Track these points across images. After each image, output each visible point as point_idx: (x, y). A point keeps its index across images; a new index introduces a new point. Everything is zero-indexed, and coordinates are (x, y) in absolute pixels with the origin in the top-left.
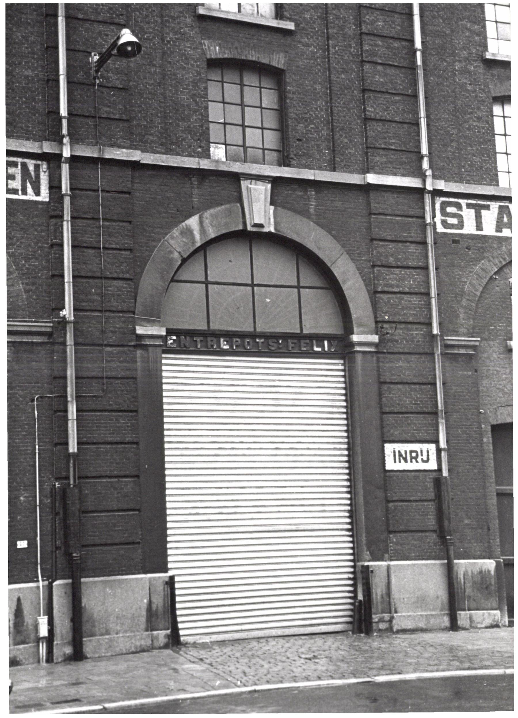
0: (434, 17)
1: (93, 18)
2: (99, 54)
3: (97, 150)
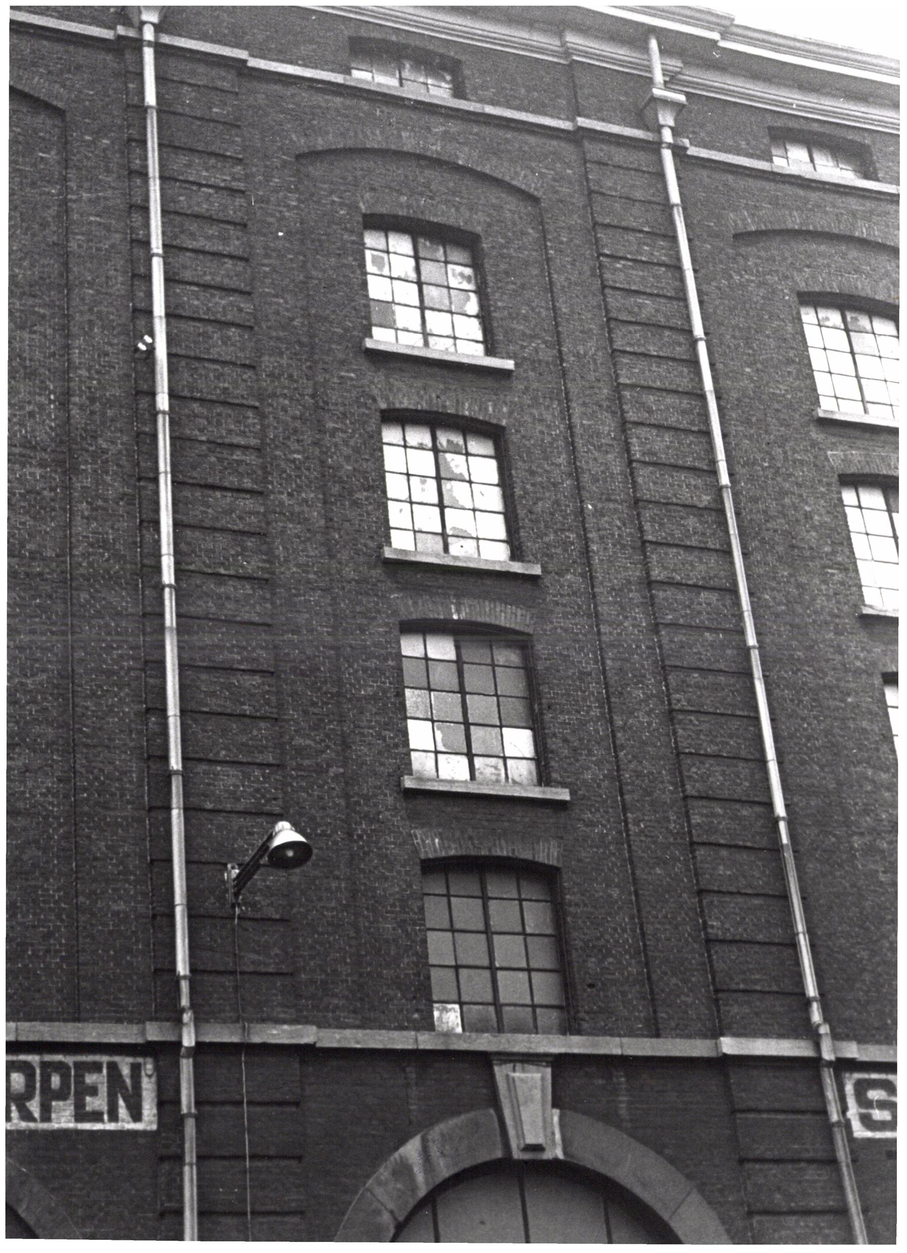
0: (803, 763)
1: (229, 807)
2: (240, 865)
3: (240, 1031)
